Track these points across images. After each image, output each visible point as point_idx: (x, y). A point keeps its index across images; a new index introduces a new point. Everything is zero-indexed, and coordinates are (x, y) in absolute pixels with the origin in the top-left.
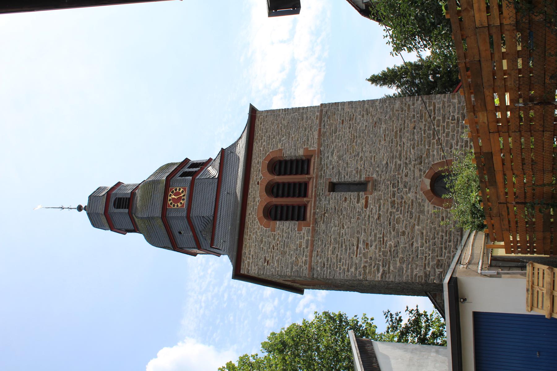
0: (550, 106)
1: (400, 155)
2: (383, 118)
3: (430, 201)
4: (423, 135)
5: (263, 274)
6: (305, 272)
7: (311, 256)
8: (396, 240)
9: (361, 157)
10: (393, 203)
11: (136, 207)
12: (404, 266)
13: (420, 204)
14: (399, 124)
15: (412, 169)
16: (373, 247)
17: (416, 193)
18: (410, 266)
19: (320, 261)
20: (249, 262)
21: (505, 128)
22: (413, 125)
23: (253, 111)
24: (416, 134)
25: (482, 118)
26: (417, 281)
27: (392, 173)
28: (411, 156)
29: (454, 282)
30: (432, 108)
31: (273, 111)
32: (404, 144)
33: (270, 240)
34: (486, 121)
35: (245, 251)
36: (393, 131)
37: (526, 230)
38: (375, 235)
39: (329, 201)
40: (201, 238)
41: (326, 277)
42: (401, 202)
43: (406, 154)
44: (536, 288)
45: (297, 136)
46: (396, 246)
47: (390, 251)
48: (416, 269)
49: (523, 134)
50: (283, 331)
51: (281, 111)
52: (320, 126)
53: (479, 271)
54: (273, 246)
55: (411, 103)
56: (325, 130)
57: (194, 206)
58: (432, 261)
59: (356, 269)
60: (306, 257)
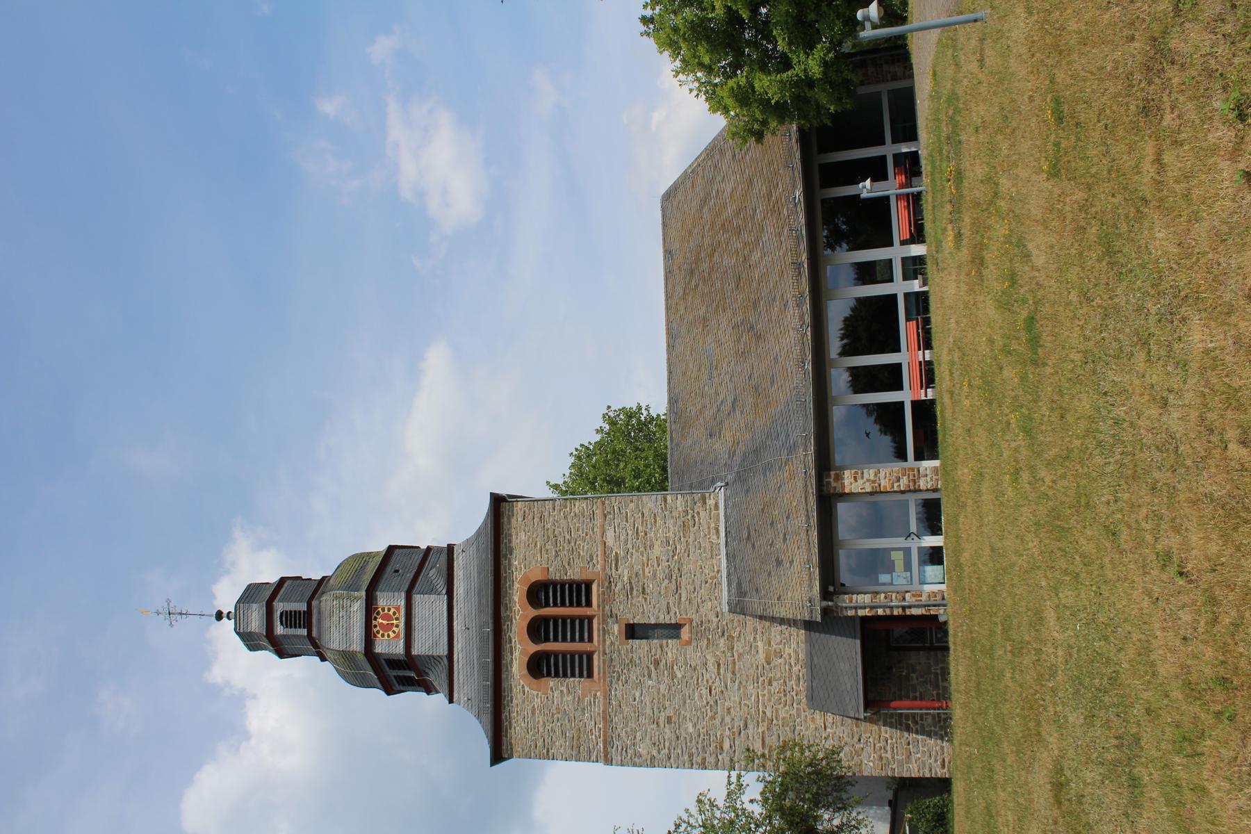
23: (499, 503)
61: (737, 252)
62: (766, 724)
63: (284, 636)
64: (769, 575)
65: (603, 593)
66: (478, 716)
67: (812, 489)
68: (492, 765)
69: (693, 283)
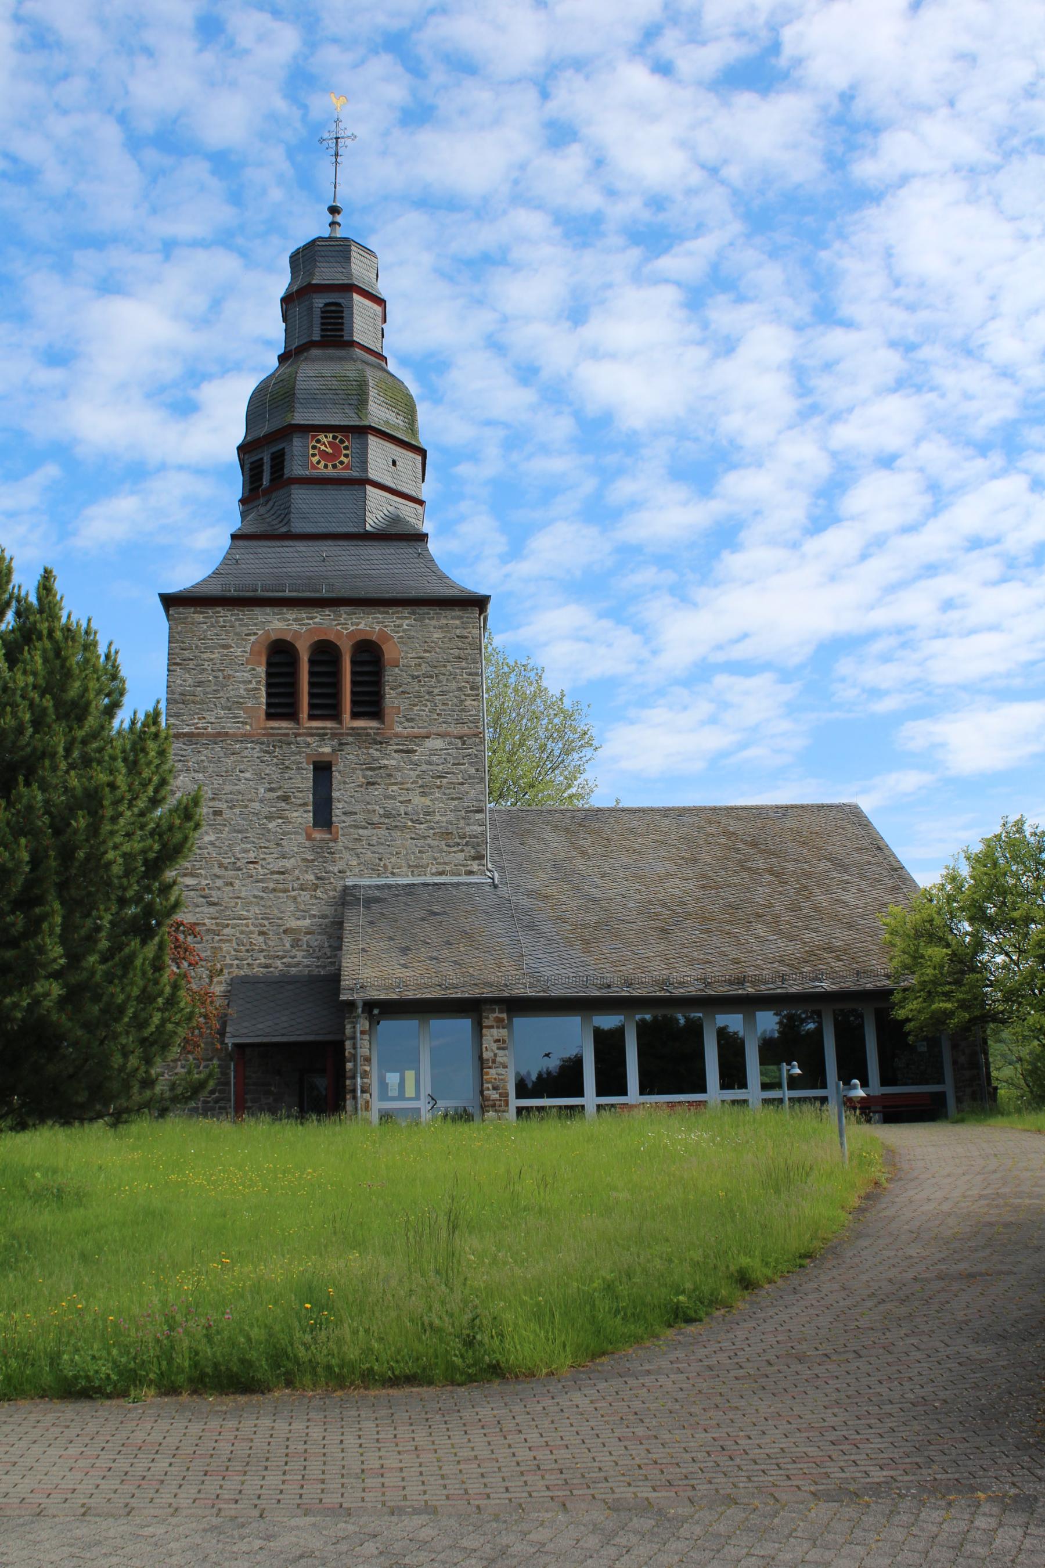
23: (480, 603)
61: (771, 906)
62: (214, 927)
63: (310, 308)
64: (391, 939)
65: (368, 735)
66: (216, 573)
67: (487, 993)
68: (160, 594)
69: (742, 846)
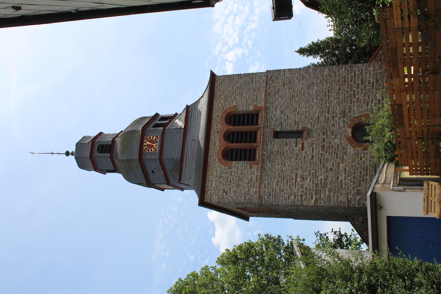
0: (438, 75)
1: (329, 110)
2: (315, 81)
3: (351, 145)
4: (346, 95)
5: (223, 202)
6: (255, 199)
7: (260, 188)
8: (325, 174)
9: (299, 112)
10: (323, 147)
11: (117, 152)
12: (332, 194)
13: (343, 147)
14: (327, 87)
15: (338, 121)
16: (308, 180)
17: (341, 139)
18: (336, 194)
19: (267, 191)
20: (211, 193)
21: (410, 88)
22: (338, 87)
23: (213, 75)
24: (341, 94)
25: (396, 82)
26: (342, 205)
27: (322, 124)
28: (337, 111)
29: (374, 196)
30: (353, 74)
31: (229, 76)
32: (331, 101)
33: (228, 175)
34: (399, 84)
35: (208, 184)
36: (323, 92)
37: (424, 158)
38: (310, 171)
39: (274, 145)
40: (170, 176)
41: (272, 203)
42: (329, 146)
43: (333, 109)
44: (430, 198)
45: (248, 96)
46: (326, 179)
47: (321, 183)
48: (341, 196)
49: (422, 92)
50: (235, 248)
51: (235, 76)
52: (266, 87)
53: (391, 188)
54: (230, 180)
55: (337, 70)
56: (270, 91)
57: (165, 150)
58: (353, 190)
59: (295, 197)
60: (256, 188)
